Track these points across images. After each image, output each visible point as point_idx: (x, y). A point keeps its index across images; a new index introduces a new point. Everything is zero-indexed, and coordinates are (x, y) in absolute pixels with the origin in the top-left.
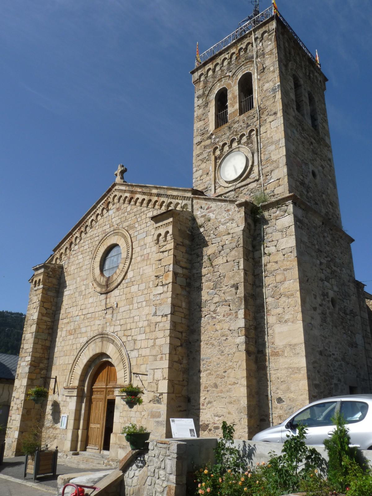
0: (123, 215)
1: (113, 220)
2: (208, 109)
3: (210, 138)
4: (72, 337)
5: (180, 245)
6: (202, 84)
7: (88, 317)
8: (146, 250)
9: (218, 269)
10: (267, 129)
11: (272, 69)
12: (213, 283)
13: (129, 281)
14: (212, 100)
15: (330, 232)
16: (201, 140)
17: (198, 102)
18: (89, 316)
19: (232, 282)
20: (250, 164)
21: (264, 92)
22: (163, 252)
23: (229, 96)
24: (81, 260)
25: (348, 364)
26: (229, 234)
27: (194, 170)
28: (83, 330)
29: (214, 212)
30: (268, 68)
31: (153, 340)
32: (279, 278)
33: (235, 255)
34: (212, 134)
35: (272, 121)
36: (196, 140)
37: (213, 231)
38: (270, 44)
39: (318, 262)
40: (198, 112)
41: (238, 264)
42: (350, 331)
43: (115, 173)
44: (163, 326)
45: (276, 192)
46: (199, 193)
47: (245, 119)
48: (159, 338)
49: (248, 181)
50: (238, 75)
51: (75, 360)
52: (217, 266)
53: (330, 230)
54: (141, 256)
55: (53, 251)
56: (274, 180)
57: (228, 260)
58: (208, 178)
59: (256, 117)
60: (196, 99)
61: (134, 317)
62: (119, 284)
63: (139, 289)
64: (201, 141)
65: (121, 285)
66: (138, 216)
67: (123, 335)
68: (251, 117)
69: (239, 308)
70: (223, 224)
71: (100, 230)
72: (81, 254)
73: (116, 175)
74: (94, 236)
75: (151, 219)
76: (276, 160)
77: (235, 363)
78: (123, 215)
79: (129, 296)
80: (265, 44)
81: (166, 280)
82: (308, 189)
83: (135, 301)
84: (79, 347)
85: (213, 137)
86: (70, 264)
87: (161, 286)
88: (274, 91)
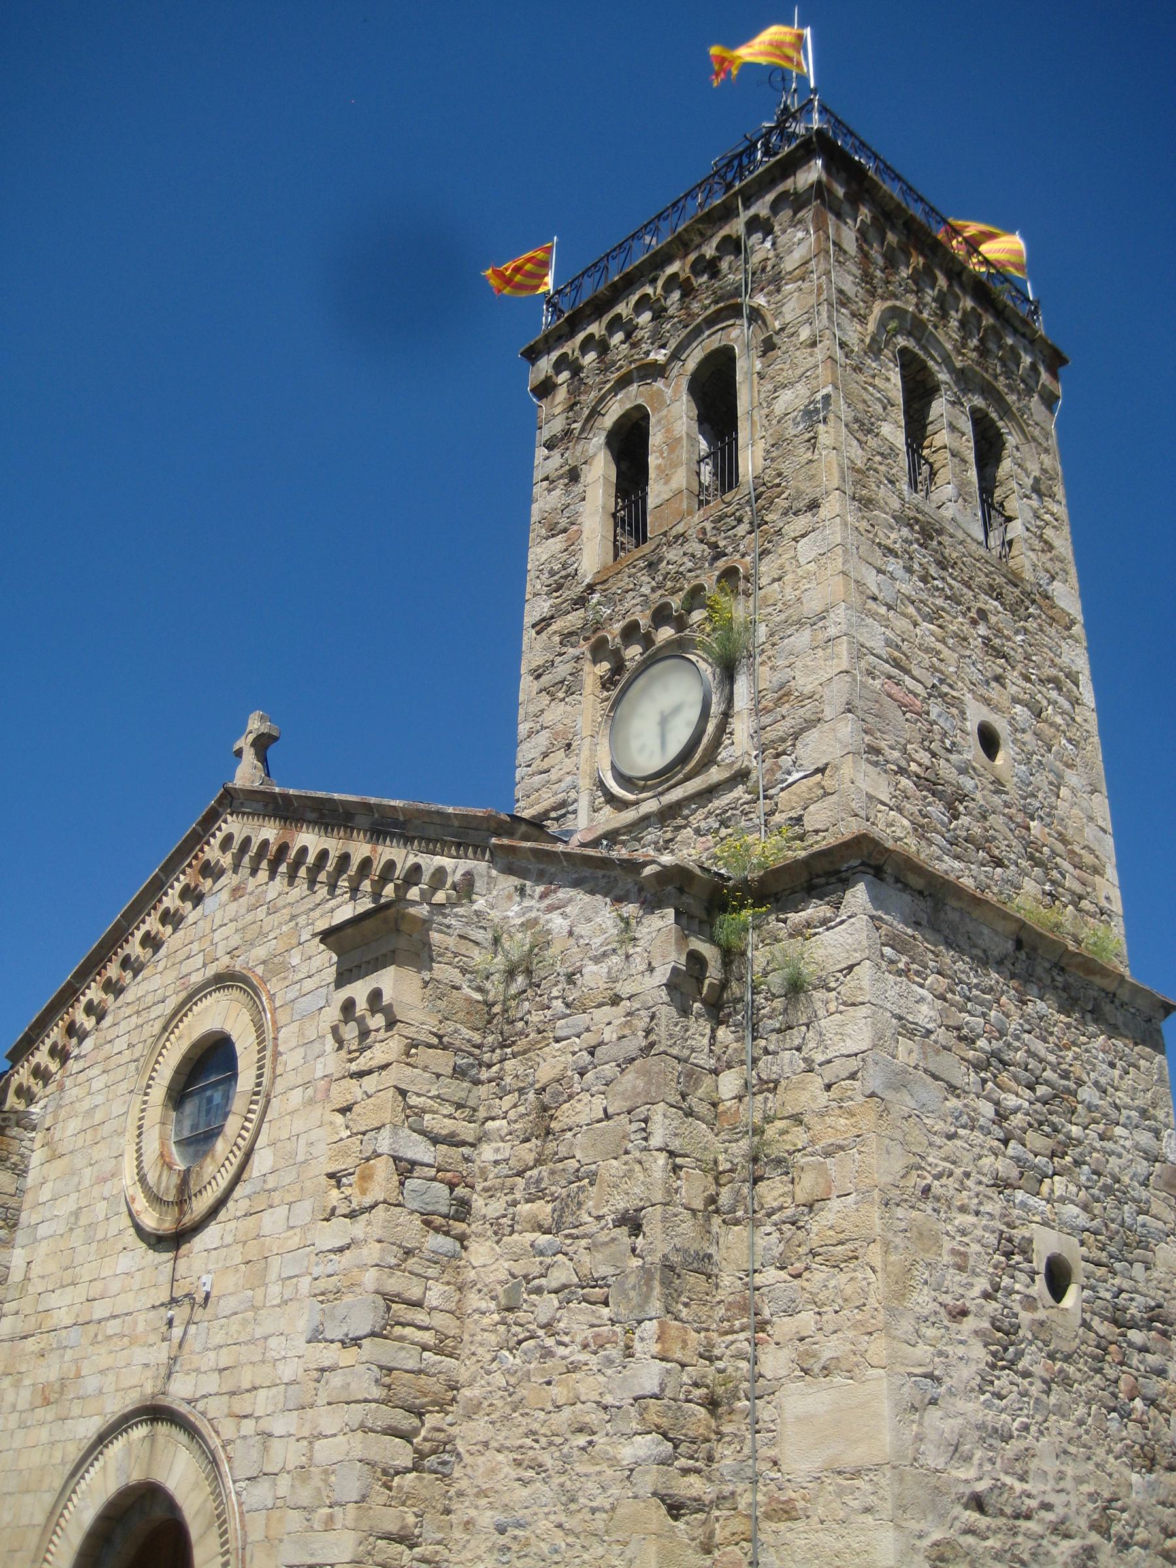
0: (249, 917)
1: (217, 936)
2: (577, 489)
3: (581, 602)
4: (48, 1413)
5: (430, 1046)
6: (561, 394)
7: (110, 1332)
8: (321, 1059)
9: (572, 1144)
10: (782, 567)
11: (805, 333)
12: (550, 1206)
13: (258, 1190)
14: (595, 455)
15: (1053, 980)
16: (550, 614)
17: (546, 462)
18: (112, 1327)
19: (621, 1203)
20: (716, 709)
21: (774, 422)
22: (360, 1075)
23: (656, 439)
24: (99, 1099)
25: (1127, 1546)
26: (615, 1000)
27: (523, 728)
28: (91, 1384)
29: (568, 910)
30: (793, 330)
31: (305, 1443)
32: (807, 1186)
33: (634, 1087)
34: (591, 588)
35: (803, 536)
36: (537, 608)
37: (560, 987)
38: (801, 241)
39: (988, 1109)
40: (544, 501)
41: (643, 1125)
42: (1144, 1399)
43: (236, 747)
44: (343, 1387)
45: (809, 824)
46: (523, 828)
47: (708, 529)
48: (326, 1437)
49: (715, 775)
50: (689, 360)
51: (52, 1513)
52: (569, 1134)
53: (1055, 972)
54: (306, 1085)
55: (8, 1057)
56: (802, 774)
57: (610, 1111)
58: (569, 764)
59: (746, 520)
60: (542, 452)
61: (266, 1338)
62: (221, 1203)
63: (291, 1224)
64: (552, 617)
65: (230, 1204)
66: (302, 920)
67: (226, 1411)
68: (728, 520)
69: (642, 1316)
70: (597, 960)
71: (171, 976)
72: (104, 1072)
73: (239, 753)
74: (150, 999)
75: (321, 941)
76: (814, 693)
77: (617, 1548)
78: (249, 917)
79: (252, 1250)
80: (782, 240)
81: (364, 1192)
82: (954, 801)
83: (273, 1275)
84: (74, 1453)
85: (596, 597)
86: (63, 1113)
87: (345, 1216)
88: (811, 418)
